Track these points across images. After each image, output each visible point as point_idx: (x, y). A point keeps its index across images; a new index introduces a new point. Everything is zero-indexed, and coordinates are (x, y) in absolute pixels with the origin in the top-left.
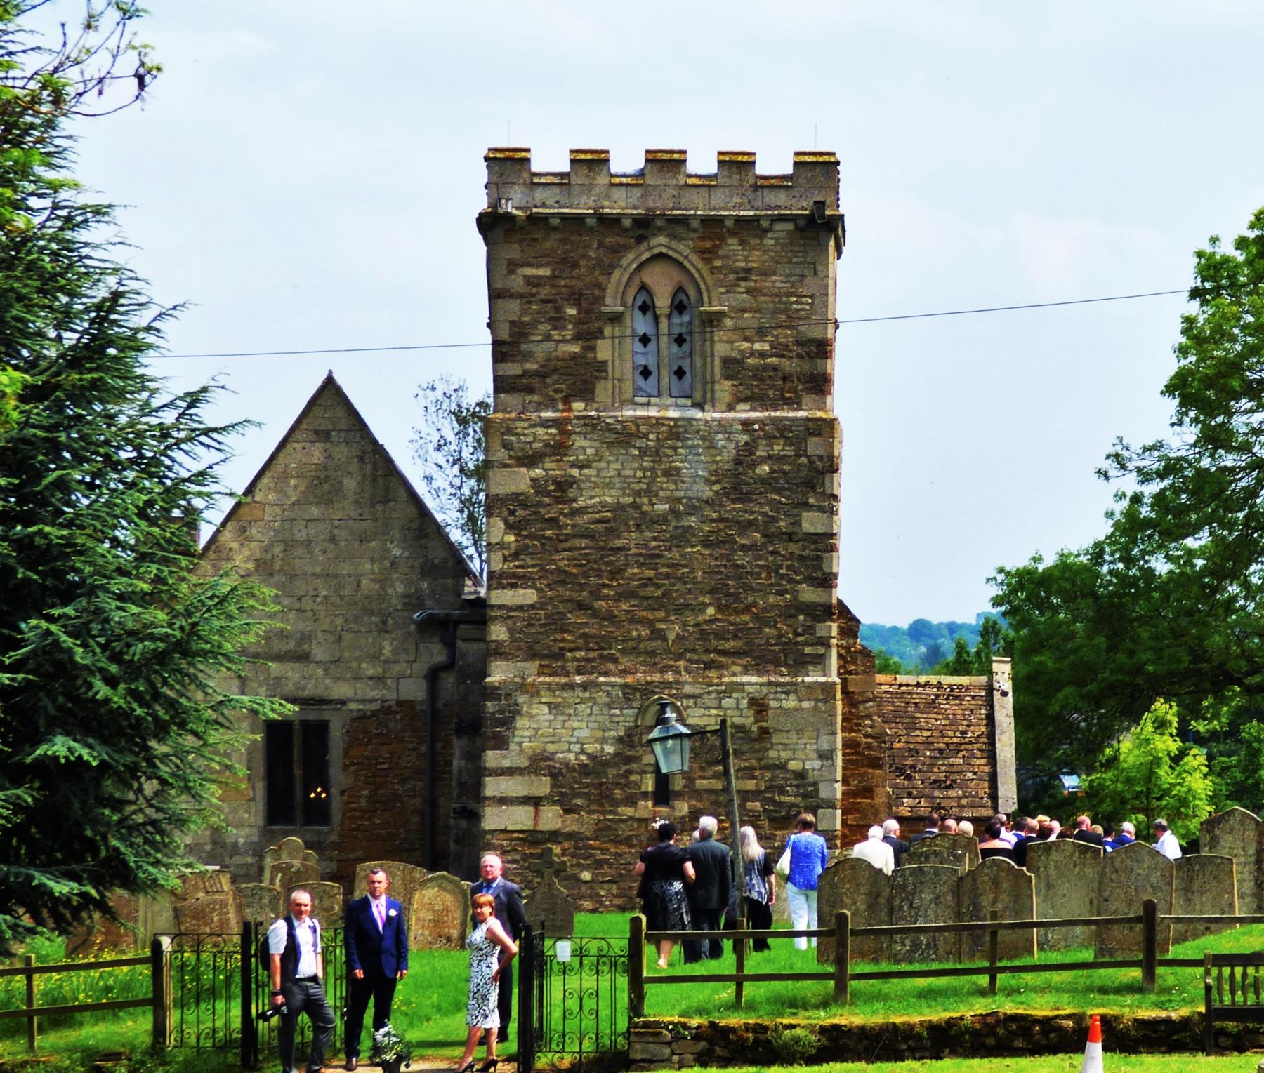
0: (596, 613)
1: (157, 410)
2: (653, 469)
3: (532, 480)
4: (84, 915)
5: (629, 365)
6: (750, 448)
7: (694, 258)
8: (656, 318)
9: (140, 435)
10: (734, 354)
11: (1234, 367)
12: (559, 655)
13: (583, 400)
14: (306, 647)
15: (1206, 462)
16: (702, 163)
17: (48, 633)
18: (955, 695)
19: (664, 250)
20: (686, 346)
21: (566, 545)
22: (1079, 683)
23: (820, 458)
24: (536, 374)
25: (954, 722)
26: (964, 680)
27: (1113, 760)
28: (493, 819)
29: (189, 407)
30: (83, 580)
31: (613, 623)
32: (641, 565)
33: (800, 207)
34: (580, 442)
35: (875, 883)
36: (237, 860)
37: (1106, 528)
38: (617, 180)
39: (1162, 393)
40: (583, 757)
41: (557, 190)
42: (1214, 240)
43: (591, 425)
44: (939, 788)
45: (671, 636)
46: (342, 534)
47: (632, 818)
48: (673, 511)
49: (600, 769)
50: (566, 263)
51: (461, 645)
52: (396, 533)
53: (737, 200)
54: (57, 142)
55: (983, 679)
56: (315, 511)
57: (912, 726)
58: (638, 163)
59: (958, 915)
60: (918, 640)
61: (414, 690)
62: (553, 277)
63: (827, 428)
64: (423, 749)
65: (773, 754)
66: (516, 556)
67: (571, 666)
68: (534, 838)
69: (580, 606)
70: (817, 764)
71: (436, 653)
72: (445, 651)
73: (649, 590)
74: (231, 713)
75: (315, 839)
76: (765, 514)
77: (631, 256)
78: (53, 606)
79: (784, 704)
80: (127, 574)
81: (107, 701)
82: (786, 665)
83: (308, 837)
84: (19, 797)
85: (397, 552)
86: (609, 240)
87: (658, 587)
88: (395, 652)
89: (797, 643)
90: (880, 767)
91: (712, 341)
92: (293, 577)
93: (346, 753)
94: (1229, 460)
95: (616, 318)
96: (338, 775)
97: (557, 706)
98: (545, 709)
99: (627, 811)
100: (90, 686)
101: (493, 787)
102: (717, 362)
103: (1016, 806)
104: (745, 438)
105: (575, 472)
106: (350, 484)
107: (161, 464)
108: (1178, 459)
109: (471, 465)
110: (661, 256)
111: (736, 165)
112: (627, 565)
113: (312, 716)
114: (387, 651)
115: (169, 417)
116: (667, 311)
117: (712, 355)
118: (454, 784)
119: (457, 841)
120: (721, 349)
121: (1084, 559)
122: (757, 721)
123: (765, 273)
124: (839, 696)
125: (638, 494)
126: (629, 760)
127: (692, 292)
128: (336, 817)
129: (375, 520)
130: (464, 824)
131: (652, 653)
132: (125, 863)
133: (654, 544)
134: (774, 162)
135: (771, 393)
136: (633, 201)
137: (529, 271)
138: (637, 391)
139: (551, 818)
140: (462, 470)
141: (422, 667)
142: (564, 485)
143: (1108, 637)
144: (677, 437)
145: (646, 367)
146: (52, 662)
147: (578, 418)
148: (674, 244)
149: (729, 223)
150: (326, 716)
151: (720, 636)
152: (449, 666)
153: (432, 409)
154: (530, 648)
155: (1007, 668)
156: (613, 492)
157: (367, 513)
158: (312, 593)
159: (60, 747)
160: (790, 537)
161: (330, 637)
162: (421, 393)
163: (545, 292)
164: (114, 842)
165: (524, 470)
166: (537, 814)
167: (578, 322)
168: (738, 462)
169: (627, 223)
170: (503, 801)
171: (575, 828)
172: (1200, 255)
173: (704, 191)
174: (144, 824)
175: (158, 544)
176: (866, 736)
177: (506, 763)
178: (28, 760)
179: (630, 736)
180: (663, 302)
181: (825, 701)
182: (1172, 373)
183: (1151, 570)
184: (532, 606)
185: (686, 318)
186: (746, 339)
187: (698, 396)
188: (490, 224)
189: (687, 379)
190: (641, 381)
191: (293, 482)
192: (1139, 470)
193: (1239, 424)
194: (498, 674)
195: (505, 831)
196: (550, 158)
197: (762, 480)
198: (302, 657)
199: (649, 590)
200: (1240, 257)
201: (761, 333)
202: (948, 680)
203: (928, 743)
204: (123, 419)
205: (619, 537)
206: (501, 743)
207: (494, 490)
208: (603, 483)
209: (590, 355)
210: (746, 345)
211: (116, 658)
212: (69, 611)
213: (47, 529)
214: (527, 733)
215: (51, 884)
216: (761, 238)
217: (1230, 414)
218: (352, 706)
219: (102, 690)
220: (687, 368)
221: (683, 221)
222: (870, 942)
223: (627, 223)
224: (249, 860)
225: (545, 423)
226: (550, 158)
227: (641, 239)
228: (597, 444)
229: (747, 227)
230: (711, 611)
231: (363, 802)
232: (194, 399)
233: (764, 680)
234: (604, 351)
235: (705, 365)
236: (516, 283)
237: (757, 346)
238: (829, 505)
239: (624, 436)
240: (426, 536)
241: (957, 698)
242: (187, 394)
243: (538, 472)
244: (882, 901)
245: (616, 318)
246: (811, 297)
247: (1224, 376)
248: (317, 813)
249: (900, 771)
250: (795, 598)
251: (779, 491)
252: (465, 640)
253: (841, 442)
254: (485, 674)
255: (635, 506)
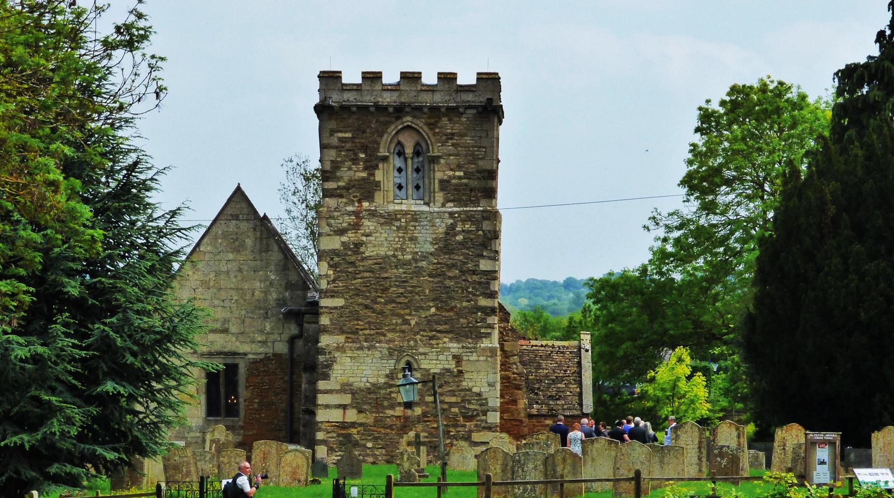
0: (374, 311)
1: (156, 219)
2: (403, 237)
3: (343, 243)
4: (120, 467)
5: (391, 183)
6: (452, 227)
7: (425, 128)
8: (406, 159)
9: (147, 232)
10: (445, 178)
11: (717, 171)
12: (355, 332)
13: (368, 201)
14: (226, 326)
15: (702, 221)
16: (430, 78)
17: (104, 330)
18: (561, 351)
19: (410, 124)
20: (421, 173)
21: (359, 276)
22: (633, 340)
23: (489, 231)
24: (344, 188)
25: (560, 366)
26: (566, 343)
27: (653, 380)
28: (322, 416)
29: (171, 217)
30: (121, 305)
31: (383, 316)
32: (397, 286)
33: (479, 99)
34: (366, 222)
35: (505, 459)
36: (192, 434)
37: (650, 256)
38: (386, 88)
39: (679, 185)
40: (368, 384)
41: (355, 93)
42: (708, 101)
43: (373, 214)
44: (552, 399)
45: (413, 323)
46: (245, 268)
47: (393, 416)
48: (413, 259)
49: (377, 391)
50: (359, 131)
51: (306, 325)
52: (272, 267)
53: (447, 98)
54: (107, 86)
55: (576, 343)
56: (231, 256)
57: (539, 367)
58: (396, 79)
59: (546, 475)
60: (569, 289)
61: (282, 348)
62: (353, 138)
63: (493, 216)
64: (286, 378)
65: (464, 383)
66: (334, 281)
67: (362, 338)
68: (343, 425)
69: (367, 307)
70: (487, 389)
71: (293, 329)
72: (298, 329)
73: (401, 300)
74: (191, 363)
75: (231, 424)
76: (461, 261)
77: (393, 127)
78: (106, 318)
79: (471, 358)
80: (142, 302)
81: (132, 364)
82: (472, 338)
83: (228, 423)
84: (89, 411)
85: (273, 277)
86: (382, 119)
87: (406, 297)
88: (272, 329)
89: (477, 327)
90: (520, 389)
91: (434, 171)
92: (220, 289)
93: (247, 381)
94: (715, 219)
95: (385, 159)
96: (243, 393)
97: (355, 358)
98: (349, 360)
99: (390, 412)
100: (124, 357)
101: (322, 399)
102: (436, 181)
103: (592, 410)
104: (452, 221)
105: (364, 239)
106: (249, 242)
107: (158, 245)
108: (689, 220)
109: (312, 204)
110: (408, 127)
111: (447, 78)
112: (391, 286)
113: (229, 361)
114: (268, 327)
115: (161, 223)
116: (411, 156)
117: (434, 178)
118: (302, 396)
119: (304, 427)
120: (439, 175)
121: (637, 274)
122: (456, 367)
123: (462, 135)
124: (499, 353)
125: (396, 250)
126: (391, 386)
127: (424, 145)
128: (242, 414)
129: (262, 260)
130: (307, 417)
131: (403, 332)
132: (141, 443)
133: (404, 275)
134: (466, 78)
135: (464, 198)
136: (394, 98)
137: (340, 135)
138: (396, 197)
139: (352, 416)
140: (307, 206)
141: (286, 336)
142: (358, 245)
143: (649, 315)
144: (416, 220)
145: (400, 184)
146: (106, 346)
147: (366, 210)
148: (415, 121)
149: (443, 110)
150: (237, 361)
151: (438, 323)
152: (300, 336)
153: (291, 172)
154: (341, 329)
155: (589, 337)
156: (383, 249)
157: (258, 257)
158: (229, 298)
159: (109, 386)
160: (474, 272)
161: (239, 321)
162: (285, 164)
163: (348, 145)
164: (136, 433)
165: (338, 237)
166: (344, 413)
167: (365, 161)
168: (447, 234)
169: (391, 110)
170: (327, 406)
171: (364, 421)
172: (700, 109)
173: (430, 94)
174: (149, 424)
175: (156, 286)
176: (514, 373)
177: (329, 388)
178: (94, 393)
179: (392, 374)
180: (409, 151)
181: (491, 357)
182: (684, 175)
183: (673, 279)
184: (342, 307)
185: (421, 159)
186: (451, 170)
187: (427, 199)
188: (321, 109)
189: (421, 190)
190: (397, 191)
191: (220, 241)
192: (667, 226)
193: (721, 199)
194: (325, 340)
195: (328, 422)
196: (351, 77)
197: (460, 243)
198: (225, 331)
199: (401, 300)
200: (722, 110)
201: (459, 167)
202: (558, 343)
203: (546, 376)
204: (139, 224)
205: (386, 272)
206: (326, 377)
207: (322, 247)
208: (379, 242)
209: (372, 178)
210: (451, 173)
211: (136, 343)
212: (114, 320)
213: (103, 280)
214: (340, 372)
215: (105, 454)
216: (460, 117)
217: (717, 195)
218: (250, 356)
219: (130, 359)
220: (421, 185)
221: (419, 109)
222: (503, 488)
223: (391, 110)
224: (198, 435)
225: (349, 214)
226: (351, 77)
227: (398, 118)
228: (375, 224)
229: (453, 112)
230: (433, 310)
231: (256, 406)
232: (174, 213)
233: (460, 345)
234: (379, 176)
235: (430, 183)
236: (334, 141)
237: (457, 174)
238: (495, 256)
239: (390, 219)
240: (288, 269)
241: (562, 353)
242: (171, 211)
243: (344, 239)
244: (509, 468)
245: (385, 159)
246: (485, 148)
247: (713, 176)
248: (232, 411)
249: (532, 390)
250: (476, 304)
251: (468, 249)
252: (308, 323)
253: (500, 223)
254: (317, 341)
255: (394, 256)
